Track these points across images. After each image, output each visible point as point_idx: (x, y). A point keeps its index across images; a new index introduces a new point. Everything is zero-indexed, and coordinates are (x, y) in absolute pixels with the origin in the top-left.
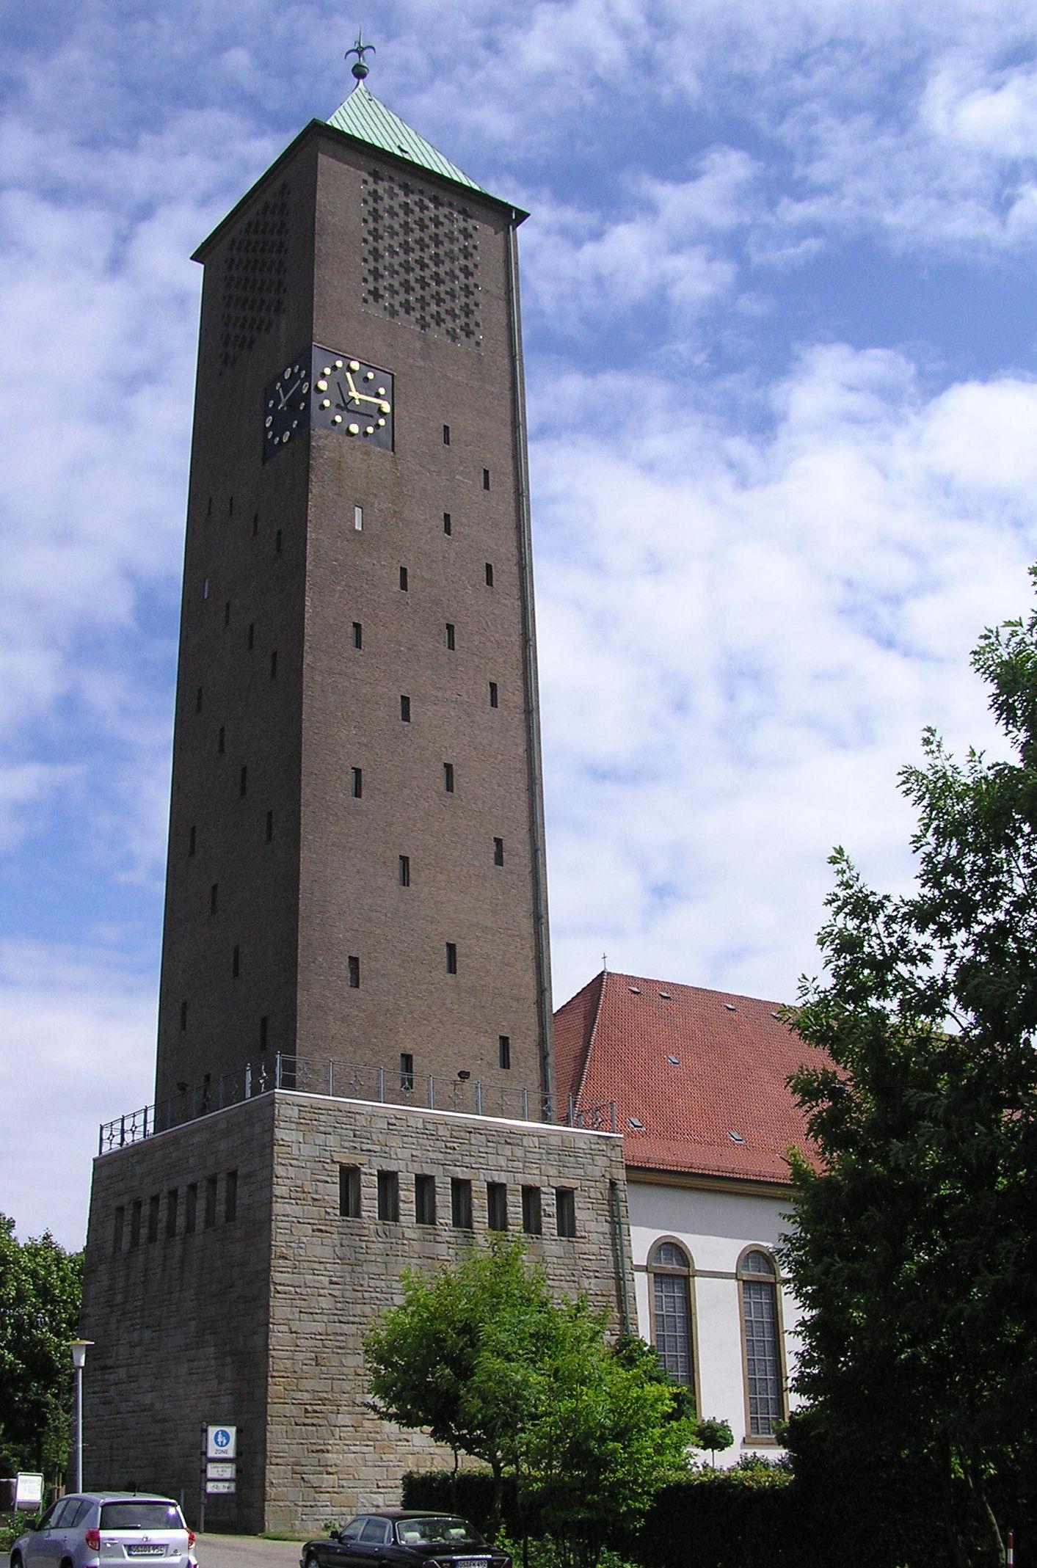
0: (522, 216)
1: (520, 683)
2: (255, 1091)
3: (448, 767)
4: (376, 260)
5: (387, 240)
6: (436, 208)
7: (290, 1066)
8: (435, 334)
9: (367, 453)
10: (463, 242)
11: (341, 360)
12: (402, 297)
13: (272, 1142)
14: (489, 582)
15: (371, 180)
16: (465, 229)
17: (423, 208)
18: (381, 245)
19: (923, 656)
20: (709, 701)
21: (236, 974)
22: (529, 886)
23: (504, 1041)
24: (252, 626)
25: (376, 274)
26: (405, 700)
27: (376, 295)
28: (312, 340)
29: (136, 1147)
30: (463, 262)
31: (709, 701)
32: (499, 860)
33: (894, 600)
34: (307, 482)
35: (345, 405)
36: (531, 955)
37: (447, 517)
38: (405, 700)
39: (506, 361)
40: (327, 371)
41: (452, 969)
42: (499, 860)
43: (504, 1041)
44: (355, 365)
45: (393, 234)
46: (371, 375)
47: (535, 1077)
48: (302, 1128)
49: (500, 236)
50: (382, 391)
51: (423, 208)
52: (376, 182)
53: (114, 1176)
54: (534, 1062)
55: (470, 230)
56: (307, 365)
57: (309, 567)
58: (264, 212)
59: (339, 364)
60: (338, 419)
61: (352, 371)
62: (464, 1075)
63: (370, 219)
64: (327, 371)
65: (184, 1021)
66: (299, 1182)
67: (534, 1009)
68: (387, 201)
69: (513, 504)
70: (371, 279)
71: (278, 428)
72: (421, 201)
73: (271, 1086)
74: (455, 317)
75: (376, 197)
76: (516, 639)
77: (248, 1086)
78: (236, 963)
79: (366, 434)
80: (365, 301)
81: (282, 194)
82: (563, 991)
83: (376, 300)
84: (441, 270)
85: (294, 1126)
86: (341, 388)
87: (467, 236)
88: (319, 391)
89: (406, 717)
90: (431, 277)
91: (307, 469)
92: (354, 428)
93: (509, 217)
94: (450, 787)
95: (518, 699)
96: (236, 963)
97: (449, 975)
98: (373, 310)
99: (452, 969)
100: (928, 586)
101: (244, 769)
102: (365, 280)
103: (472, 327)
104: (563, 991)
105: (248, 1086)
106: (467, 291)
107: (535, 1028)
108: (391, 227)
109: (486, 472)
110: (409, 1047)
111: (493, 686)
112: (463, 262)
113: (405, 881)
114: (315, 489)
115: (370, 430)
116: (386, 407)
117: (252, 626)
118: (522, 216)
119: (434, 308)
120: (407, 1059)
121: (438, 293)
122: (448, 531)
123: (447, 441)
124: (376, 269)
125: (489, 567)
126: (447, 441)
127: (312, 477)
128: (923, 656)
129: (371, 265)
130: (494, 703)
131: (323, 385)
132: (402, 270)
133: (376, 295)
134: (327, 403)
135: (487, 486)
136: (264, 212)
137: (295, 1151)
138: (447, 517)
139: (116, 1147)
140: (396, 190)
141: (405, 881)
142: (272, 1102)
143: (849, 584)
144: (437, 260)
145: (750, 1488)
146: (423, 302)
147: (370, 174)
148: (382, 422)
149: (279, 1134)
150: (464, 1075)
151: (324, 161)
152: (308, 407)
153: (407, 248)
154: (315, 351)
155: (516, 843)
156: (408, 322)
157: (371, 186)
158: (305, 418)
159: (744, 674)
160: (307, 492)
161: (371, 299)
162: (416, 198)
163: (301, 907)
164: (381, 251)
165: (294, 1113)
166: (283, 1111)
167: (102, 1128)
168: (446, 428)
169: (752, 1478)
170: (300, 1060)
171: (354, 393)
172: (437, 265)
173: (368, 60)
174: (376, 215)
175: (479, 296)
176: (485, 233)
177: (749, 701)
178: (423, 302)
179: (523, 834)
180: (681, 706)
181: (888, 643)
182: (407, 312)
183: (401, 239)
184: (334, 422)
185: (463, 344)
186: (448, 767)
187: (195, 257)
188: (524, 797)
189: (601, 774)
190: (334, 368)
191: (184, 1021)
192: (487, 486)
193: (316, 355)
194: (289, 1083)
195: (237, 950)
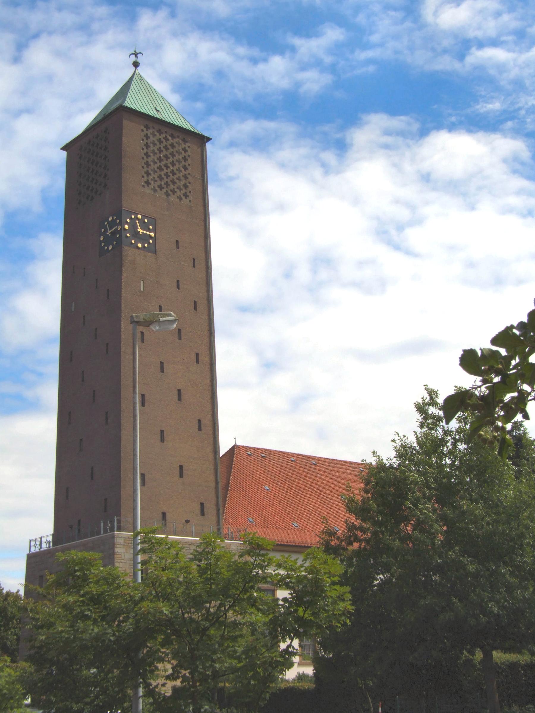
0: (208, 139)
1: (208, 352)
2: (105, 531)
3: (179, 391)
4: (147, 167)
5: (152, 157)
6: (172, 139)
7: (119, 522)
8: (173, 198)
9: (145, 256)
10: (183, 154)
11: (129, 198)
12: (158, 183)
13: (114, 553)
14: (195, 308)
15: (145, 129)
16: (185, 148)
17: (167, 140)
18: (150, 160)
19: (416, 255)
20: (303, 274)
21: (92, 478)
22: (212, 439)
23: (202, 505)
24: (96, 329)
25: (148, 174)
26: (162, 363)
27: (148, 183)
28: (121, 207)
29: (44, 551)
30: (184, 163)
31: (303, 274)
32: (200, 429)
33: (400, 228)
34: (121, 271)
35: (136, 234)
36: (213, 468)
37: (178, 281)
38: (162, 363)
39: (202, 208)
40: (128, 220)
41: (181, 475)
42: (200, 429)
43: (202, 505)
44: (140, 216)
45: (155, 153)
46: (146, 221)
47: (214, 519)
48: (125, 547)
49: (199, 150)
50: (151, 227)
51: (167, 140)
52: (147, 130)
53: (36, 563)
54: (214, 512)
55: (187, 148)
56: (119, 217)
57: (122, 309)
58: (97, 137)
59: (133, 217)
60: (133, 242)
61: (138, 219)
62: (187, 521)
63: (145, 148)
64: (128, 220)
65: (67, 496)
66: (124, 569)
67: (214, 491)
68: (152, 139)
69: (205, 273)
70: (145, 175)
71: (107, 241)
72: (166, 136)
73: (112, 530)
74: (180, 189)
75: (147, 137)
76: (206, 332)
77: (102, 529)
78: (92, 473)
79: (145, 247)
80: (143, 186)
81: (105, 132)
82: (224, 448)
83: (148, 186)
84: (175, 168)
85: (122, 546)
86: (133, 227)
87: (185, 150)
88: (125, 229)
89: (162, 370)
90: (171, 172)
91: (121, 265)
92: (140, 245)
93: (202, 140)
94: (180, 399)
95: (207, 359)
96: (92, 473)
97: (180, 479)
98: (147, 190)
99: (181, 475)
100: (417, 221)
101: (94, 391)
102: (143, 177)
103: (188, 194)
104: (224, 448)
105: (102, 529)
106: (186, 177)
107: (215, 499)
108: (154, 150)
109: (194, 259)
110: (165, 509)
111: (197, 354)
112: (184, 163)
113: (162, 440)
114: (124, 274)
115: (146, 245)
116: (152, 234)
117: (96, 329)
118: (208, 139)
119: (172, 186)
120: (164, 515)
121: (173, 179)
122: (178, 287)
123: (178, 247)
124: (148, 171)
125: (195, 302)
126: (178, 247)
127: (123, 269)
128: (416, 255)
129: (146, 169)
130: (197, 362)
131: (127, 227)
132: (158, 170)
133: (148, 183)
134: (128, 235)
135: (194, 266)
136: (97, 137)
137: (123, 556)
138: (178, 281)
139: (37, 550)
140: (156, 133)
141: (162, 440)
142: (113, 537)
143: (378, 218)
144: (173, 164)
145: (301, 690)
146: (167, 184)
147: (145, 127)
148: (151, 241)
149: (117, 550)
150: (187, 521)
151: (125, 123)
152: (120, 236)
153: (160, 160)
154: (123, 211)
155: (207, 422)
156: (161, 194)
157: (145, 132)
158: (119, 242)
159: (322, 261)
160: (121, 275)
161: (146, 185)
162: (164, 135)
163: (122, 454)
164: (150, 163)
165: (122, 541)
166: (119, 541)
167: (30, 541)
168: (177, 241)
169: (301, 686)
170: (122, 519)
171: (139, 230)
172: (173, 166)
173: (140, 59)
174: (147, 146)
175: (190, 179)
176: (192, 147)
177: (323, 274)
178: (167, 184)
179: (209, 417)
180: (288, 275)
181: (397, 248)
182: (161, 190)
183: (158, 156)
184: (132, 243)
185: (185, 201)
186: (179, 391)
187: (63, 149)
188: (210, 401)
189: (244, 309)
190: (131, 219)
191: (67, 496)
192: (194, 266)
193: (124, 214)
194: (119, 529)
195: (92, 468)
